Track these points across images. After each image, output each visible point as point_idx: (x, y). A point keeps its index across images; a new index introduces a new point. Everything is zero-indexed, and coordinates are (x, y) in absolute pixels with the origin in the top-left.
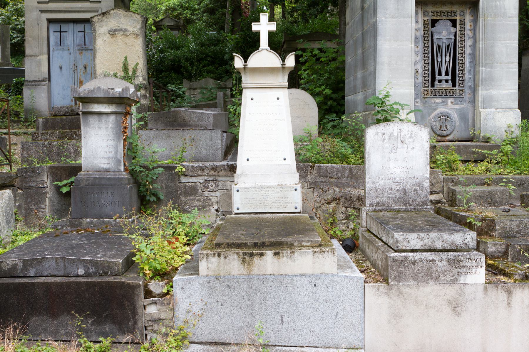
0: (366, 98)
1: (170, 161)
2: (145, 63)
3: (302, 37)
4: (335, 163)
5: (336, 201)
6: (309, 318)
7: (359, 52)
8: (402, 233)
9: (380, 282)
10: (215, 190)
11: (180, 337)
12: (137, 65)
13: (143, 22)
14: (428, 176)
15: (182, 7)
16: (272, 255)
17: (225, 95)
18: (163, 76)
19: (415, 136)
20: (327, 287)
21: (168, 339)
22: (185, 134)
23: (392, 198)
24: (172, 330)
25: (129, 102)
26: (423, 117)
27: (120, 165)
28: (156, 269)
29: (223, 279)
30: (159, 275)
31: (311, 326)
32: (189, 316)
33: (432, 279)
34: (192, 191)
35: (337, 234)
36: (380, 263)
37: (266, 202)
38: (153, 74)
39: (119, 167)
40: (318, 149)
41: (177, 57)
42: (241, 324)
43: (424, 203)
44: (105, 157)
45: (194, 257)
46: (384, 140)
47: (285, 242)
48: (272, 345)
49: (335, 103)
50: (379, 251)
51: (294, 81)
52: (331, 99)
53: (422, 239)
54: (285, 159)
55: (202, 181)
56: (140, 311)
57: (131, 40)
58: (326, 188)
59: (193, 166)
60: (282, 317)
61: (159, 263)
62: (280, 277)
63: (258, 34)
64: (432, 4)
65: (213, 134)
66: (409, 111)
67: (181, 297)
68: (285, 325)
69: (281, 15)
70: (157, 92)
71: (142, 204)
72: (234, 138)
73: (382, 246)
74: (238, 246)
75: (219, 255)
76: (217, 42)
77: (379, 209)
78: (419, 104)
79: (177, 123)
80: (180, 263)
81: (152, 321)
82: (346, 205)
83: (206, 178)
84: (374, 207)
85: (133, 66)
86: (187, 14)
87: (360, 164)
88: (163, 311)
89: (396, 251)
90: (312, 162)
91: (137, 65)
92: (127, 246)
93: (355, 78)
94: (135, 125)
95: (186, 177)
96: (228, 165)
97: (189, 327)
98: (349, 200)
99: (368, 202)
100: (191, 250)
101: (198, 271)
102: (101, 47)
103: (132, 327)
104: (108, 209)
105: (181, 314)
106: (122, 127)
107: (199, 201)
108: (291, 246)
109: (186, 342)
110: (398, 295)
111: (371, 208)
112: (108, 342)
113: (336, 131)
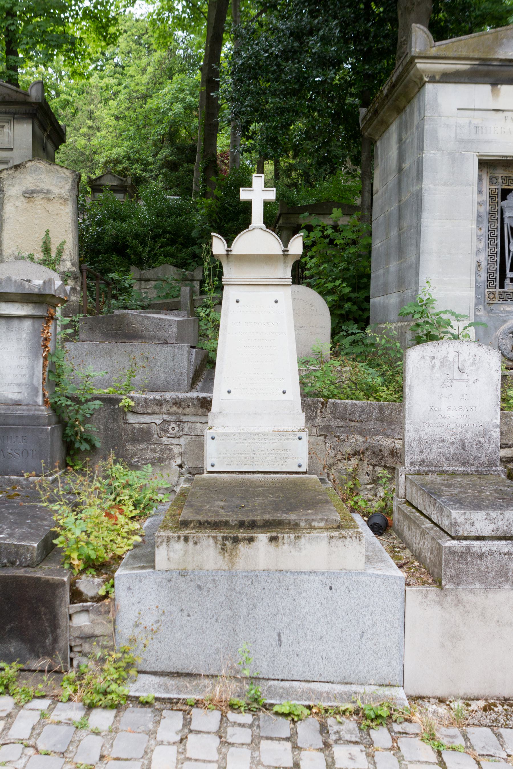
0: (402, 303)
1: (112, 389)
2: (76, 241)
3: (304, 209)
4: (357, 399)
5: (359, 455)
6: (321, 637)
7: (394, 233)
8: (463, 511)
9: (428, 584)
10: (178, 435)
11: (122, 664)
12: (64, 243)
13: (74, 181)
14: (498, 423)
15: (129, 159)
16: (267, 541)
17: (192, 292)
18: (100, 260)
19: (479, 362)
20: (349, 591)
21: (105, 667)
22: (134, 349)
23: (444, 455)
24: (111, 653)
25: (54, 301)
26: (487, 332)
27: (36, 395)
28: (88, 557)
29: (192, 576)
30: (94, 567)
31: (323, 650)
32: (137, 631)
33: (507, 581)
34: (144, 436)
35: (359, 506)
36: (428, 555)
37: (255, 456)
38: (86, 257)
39: (35, 399)
40: (332, 376)
41: (122, 232)
42: (218, 645)
43: (491, 463)
44: (15, 382)
45: (146, 539)
46: (433, 367)
47: (287, 521)
48: (263, 679)
49: (356, 307)
50: (426, 536)
51: (299, 274)
52: (349, 299)
53: (493, 521)
54: (284, 392)
55: (158, 422)
56: (63, 622)
57: (56, 207)
58: (343, 436)
59: (146, 399)
60: (279, 635)
61: (93, 549)
62: (278, 574)
63: (248, 205)
64: (503, 166)
65: (176, 351)
66: (467, 323)
67: (126, 602)
68: (284, 648)
69: (273, 174)
70: (91, 284)
71: (68, 454)
72: (205, 356)
73: (432, 529)
74: (216, 525)
75: (186, 539)
76: (180, 210)
77: (424, 471)
78: (481, 313)
79: (122, 333)
80: (126, 548)
81: (82, 638)
82: (374, 462)
83: (165, 417)
84: (417, 468)
85: (57, 245)
86: (137, 169)
87: (395, 401)
88: (98, 624)
89: (453, 538)
90: (323, 396)
91: (64, 243)
92: (45, 520)
93: (387, 272)
94: (60, 333)
95: (135, 416)
96: (198, 398)
97: (137, 649)
98: (378, 455)
99: (408, 460)
100: (141, 528)
101: (154, 561)
102: (11, 215)
103: (51, 648)
104: (17, 461)
105: (125, 628)
106: (42, 339)
107: (154, 451)
108: (295, 527)
109: (133, 672)
110: (456, 605)
111: (412, 469)
112: (13, 670)
113: (358, 350)
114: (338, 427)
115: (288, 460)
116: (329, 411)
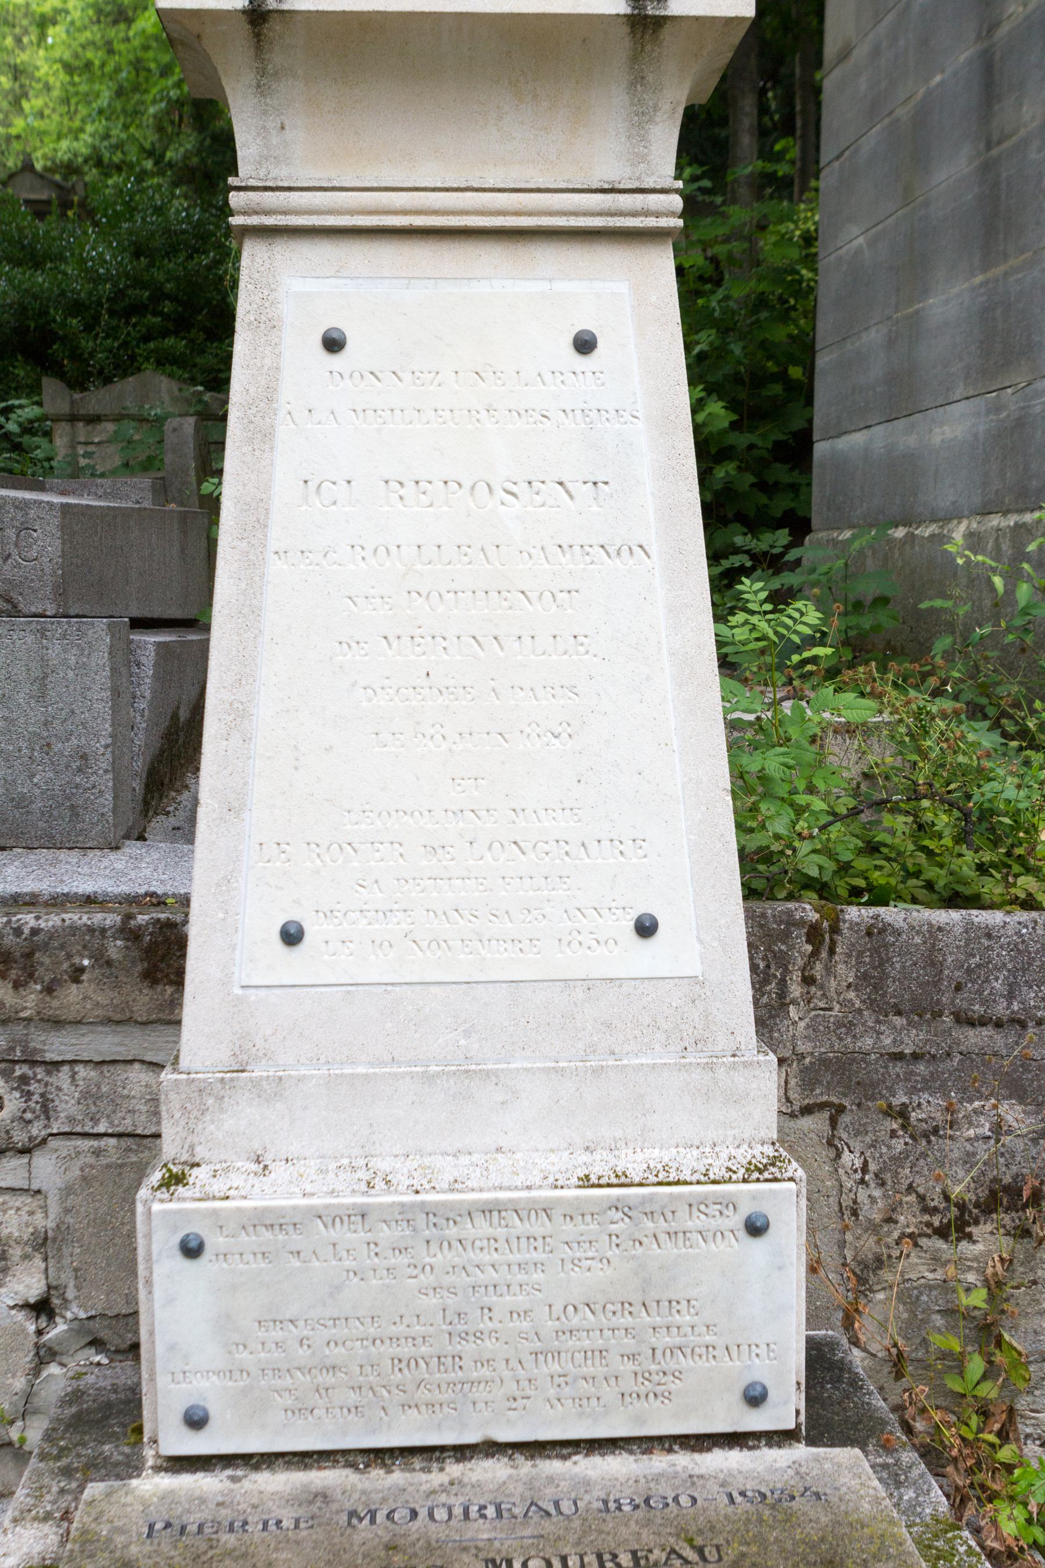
10: (20, 1138)
15: (99, 163)
37: (469, 1348)
41: (35, 297)
58: (928, 1108)
65: (54, 651)
114: (898, 1057)
115: (683, 1362)
116: (845, 973)
